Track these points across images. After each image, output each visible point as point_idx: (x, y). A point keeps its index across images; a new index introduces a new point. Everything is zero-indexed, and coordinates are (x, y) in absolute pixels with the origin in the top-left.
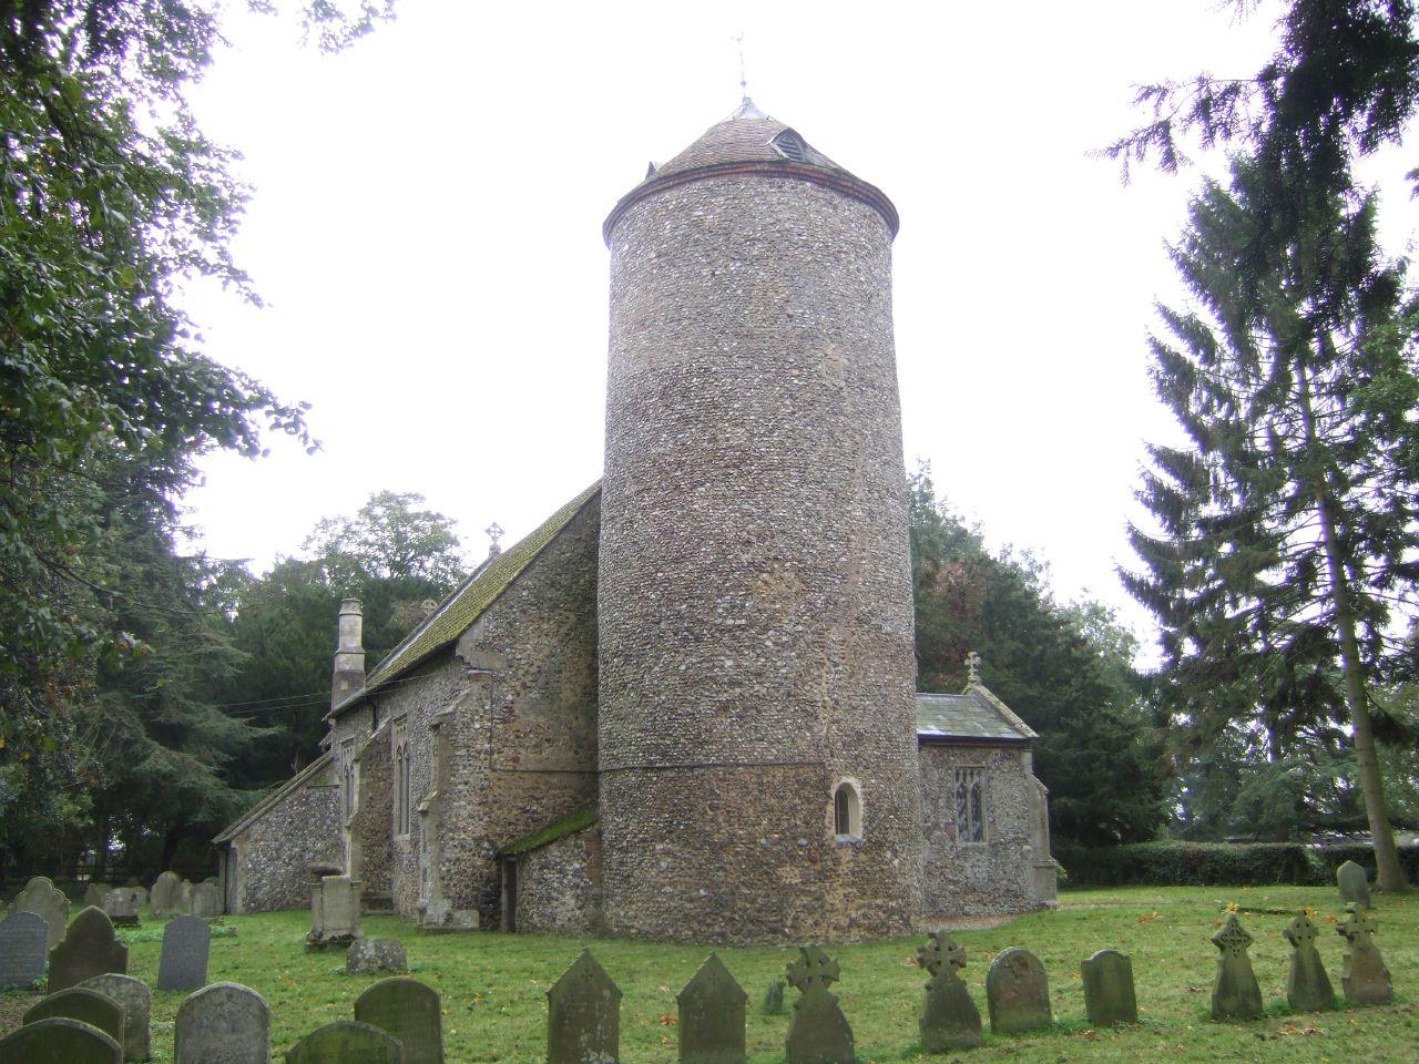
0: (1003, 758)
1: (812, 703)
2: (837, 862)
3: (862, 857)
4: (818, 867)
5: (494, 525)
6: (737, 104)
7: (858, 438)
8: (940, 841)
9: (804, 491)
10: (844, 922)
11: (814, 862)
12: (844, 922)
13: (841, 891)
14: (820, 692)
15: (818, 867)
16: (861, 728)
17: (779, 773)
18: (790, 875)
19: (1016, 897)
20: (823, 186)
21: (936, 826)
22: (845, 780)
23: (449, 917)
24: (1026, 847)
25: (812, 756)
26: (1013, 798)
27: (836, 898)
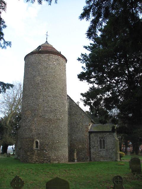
0: (109, 135)
1: (32, 129)
2: (34, 152)
3: (39, 151)
4: (32, 152)
5: (78, 102)
6: (45, 42)
7: (42, 89)
8: (95, 149)
9: (32, 99)
10: (35, 161)
11: (31, 152)
12: (35, 161)
13: (35, 156)
14: (33, 128)
15: (32, 152)
16: (39, 132)
17: (28, 139)
18: (29, 153)
19: (111, 158)
20: (38, 54)
21: (95, 146)
22: (36, 140)
23: (17, 158)
24: (114, 150)
25: (32, 137)
26: (111, 141)
27: (34, 157)
